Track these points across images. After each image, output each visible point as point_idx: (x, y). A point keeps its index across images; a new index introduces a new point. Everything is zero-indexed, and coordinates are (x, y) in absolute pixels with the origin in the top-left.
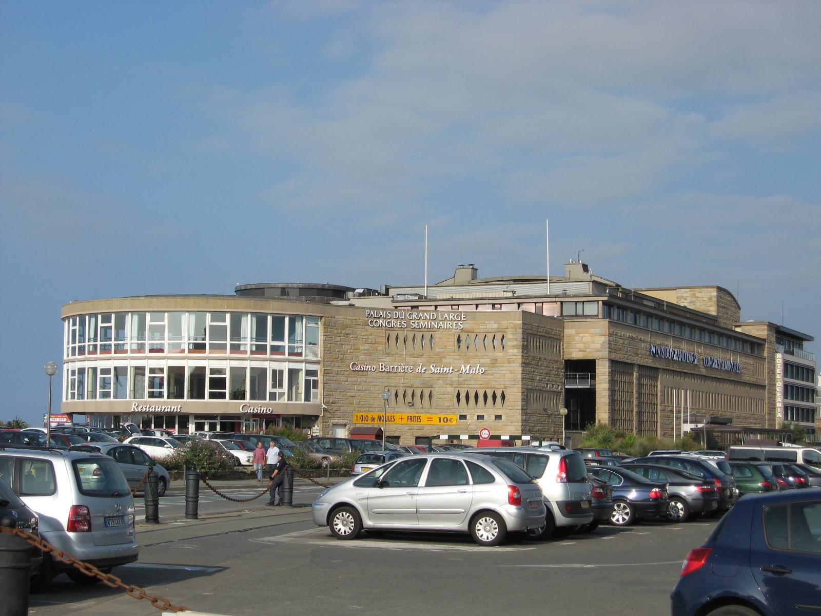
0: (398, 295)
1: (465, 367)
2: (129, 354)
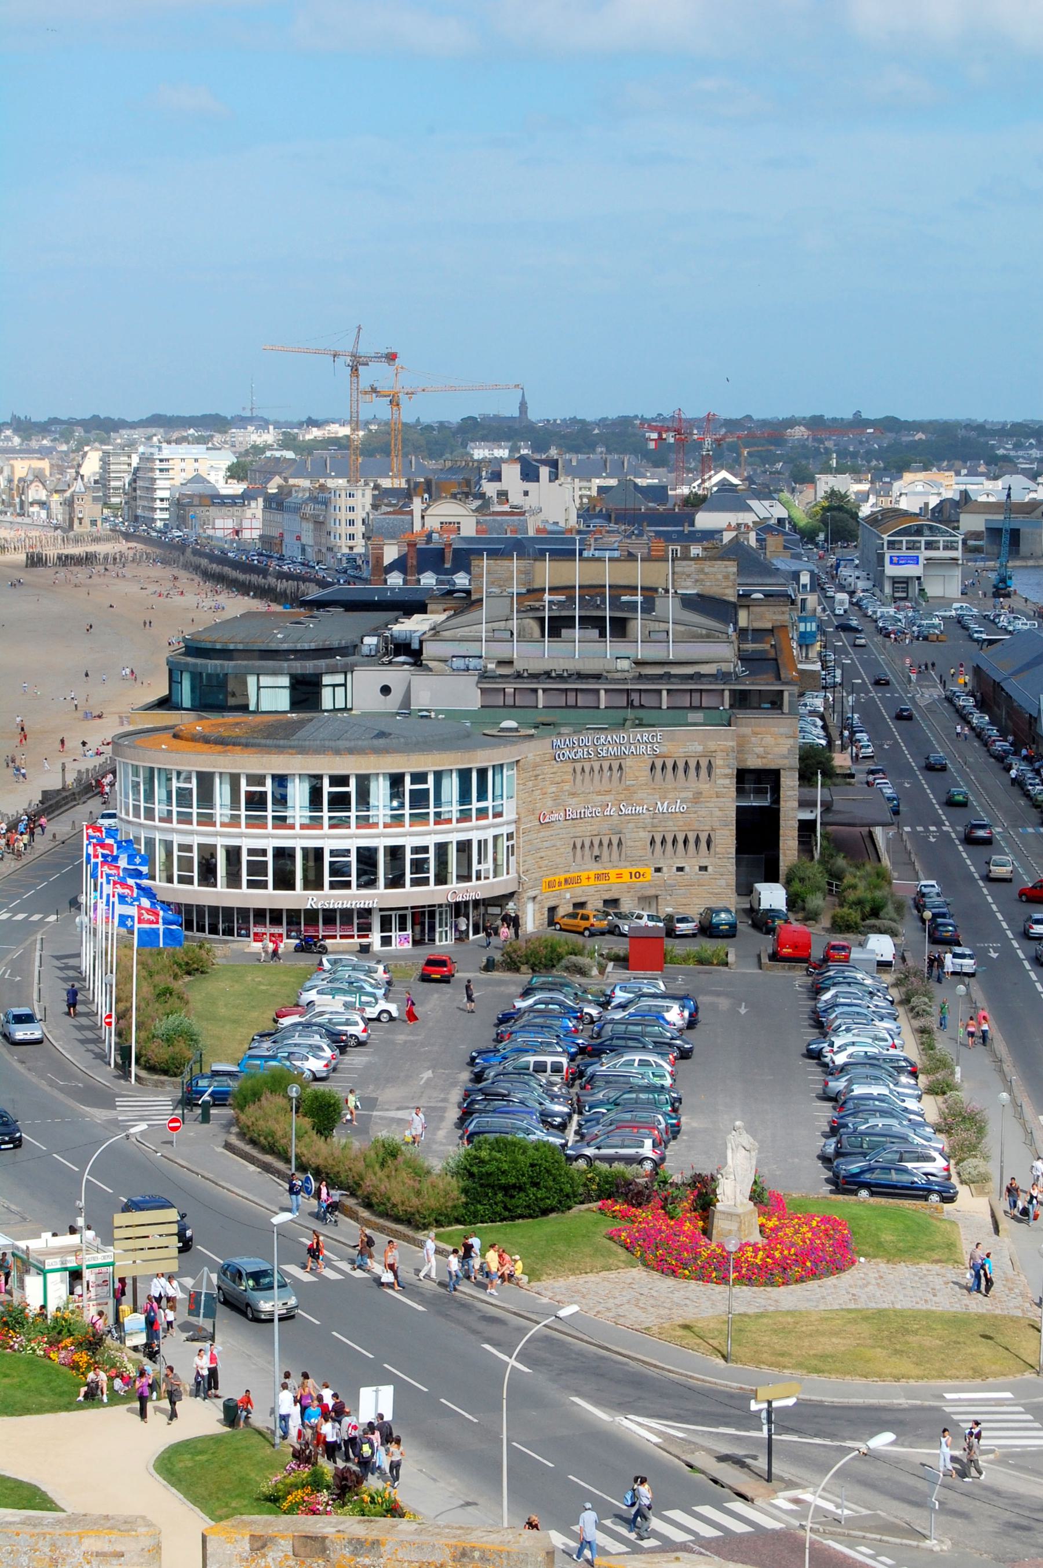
0: (454, 657)
1: (662, 804)
2: (297, 830)
